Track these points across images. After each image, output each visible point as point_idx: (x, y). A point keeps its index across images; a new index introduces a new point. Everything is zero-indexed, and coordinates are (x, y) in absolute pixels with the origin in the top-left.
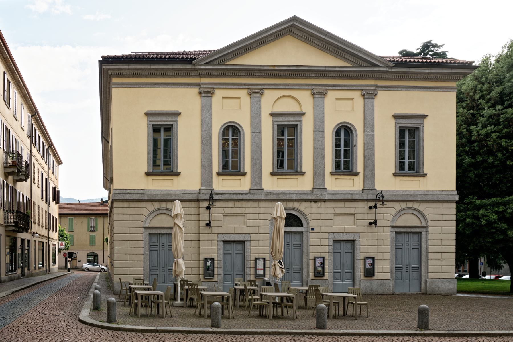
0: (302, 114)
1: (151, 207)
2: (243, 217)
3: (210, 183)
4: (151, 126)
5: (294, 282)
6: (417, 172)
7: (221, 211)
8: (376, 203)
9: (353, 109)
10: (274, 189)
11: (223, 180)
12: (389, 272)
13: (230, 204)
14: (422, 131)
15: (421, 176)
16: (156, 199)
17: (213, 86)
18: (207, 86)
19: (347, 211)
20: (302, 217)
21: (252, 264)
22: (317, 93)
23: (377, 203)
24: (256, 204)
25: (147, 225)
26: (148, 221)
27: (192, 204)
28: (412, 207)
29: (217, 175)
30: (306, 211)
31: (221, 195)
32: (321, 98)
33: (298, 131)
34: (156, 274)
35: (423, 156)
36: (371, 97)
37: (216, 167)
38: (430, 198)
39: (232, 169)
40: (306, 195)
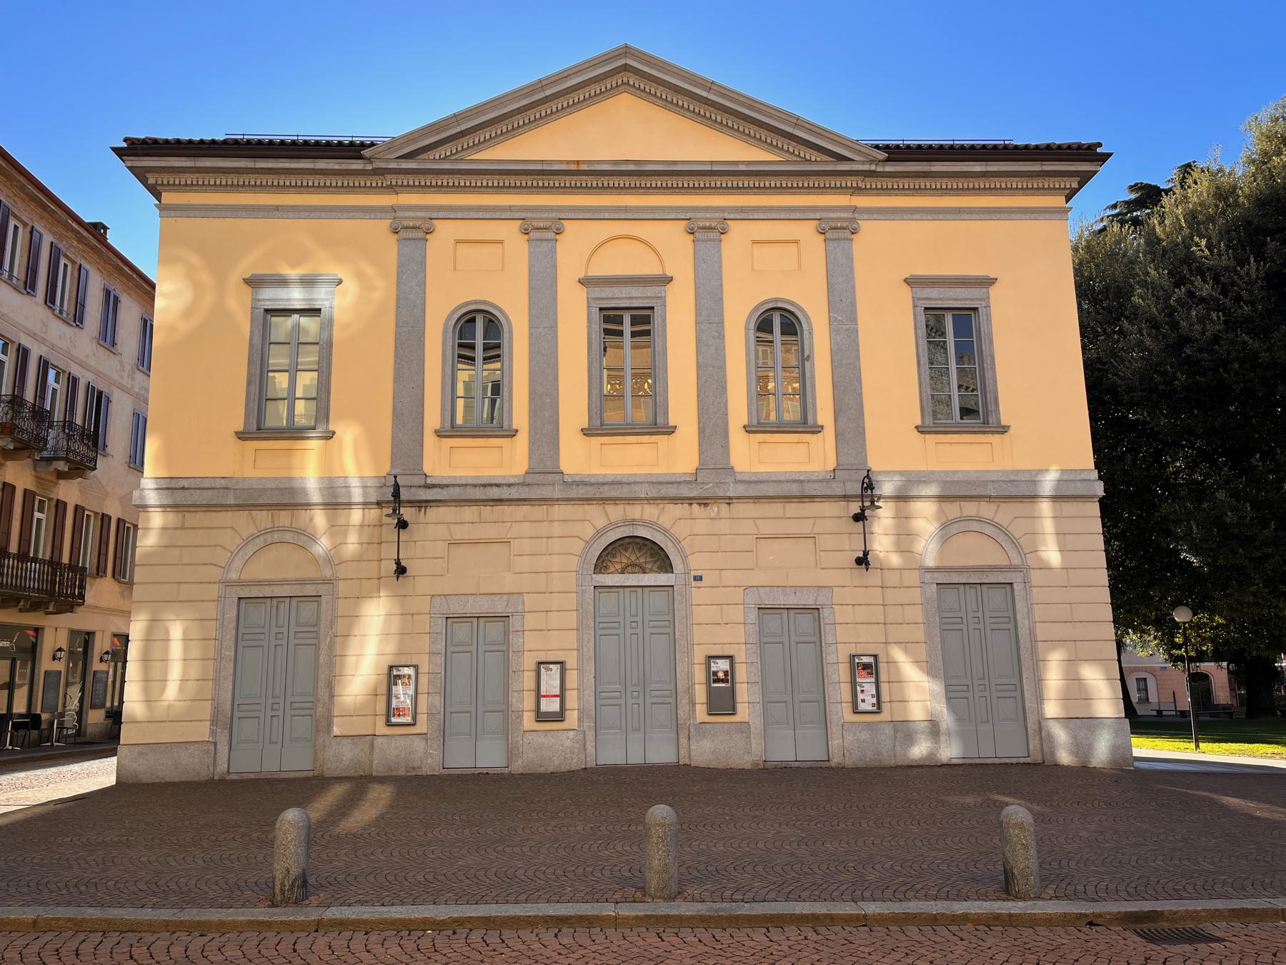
1: (244, 523)
4: (595, 311)
6: (986, 422)
7: (442, 531)
9: (800, 268)
13: (469, 513)
14: (985, 318)
15: (993, 433)
16: (261, 501)
17: (430, 215)
18: (412, 214)
19: (792, 527)
20: (670, 544)
24: (539, 512)
25: (234, 576)
26: (238, 563)
30: (680, 530)
31: (439, 490)
33: (656, 322)
35: (996, 382)
36: (841, 234)
37: (433, 418)
40: (675, 485)
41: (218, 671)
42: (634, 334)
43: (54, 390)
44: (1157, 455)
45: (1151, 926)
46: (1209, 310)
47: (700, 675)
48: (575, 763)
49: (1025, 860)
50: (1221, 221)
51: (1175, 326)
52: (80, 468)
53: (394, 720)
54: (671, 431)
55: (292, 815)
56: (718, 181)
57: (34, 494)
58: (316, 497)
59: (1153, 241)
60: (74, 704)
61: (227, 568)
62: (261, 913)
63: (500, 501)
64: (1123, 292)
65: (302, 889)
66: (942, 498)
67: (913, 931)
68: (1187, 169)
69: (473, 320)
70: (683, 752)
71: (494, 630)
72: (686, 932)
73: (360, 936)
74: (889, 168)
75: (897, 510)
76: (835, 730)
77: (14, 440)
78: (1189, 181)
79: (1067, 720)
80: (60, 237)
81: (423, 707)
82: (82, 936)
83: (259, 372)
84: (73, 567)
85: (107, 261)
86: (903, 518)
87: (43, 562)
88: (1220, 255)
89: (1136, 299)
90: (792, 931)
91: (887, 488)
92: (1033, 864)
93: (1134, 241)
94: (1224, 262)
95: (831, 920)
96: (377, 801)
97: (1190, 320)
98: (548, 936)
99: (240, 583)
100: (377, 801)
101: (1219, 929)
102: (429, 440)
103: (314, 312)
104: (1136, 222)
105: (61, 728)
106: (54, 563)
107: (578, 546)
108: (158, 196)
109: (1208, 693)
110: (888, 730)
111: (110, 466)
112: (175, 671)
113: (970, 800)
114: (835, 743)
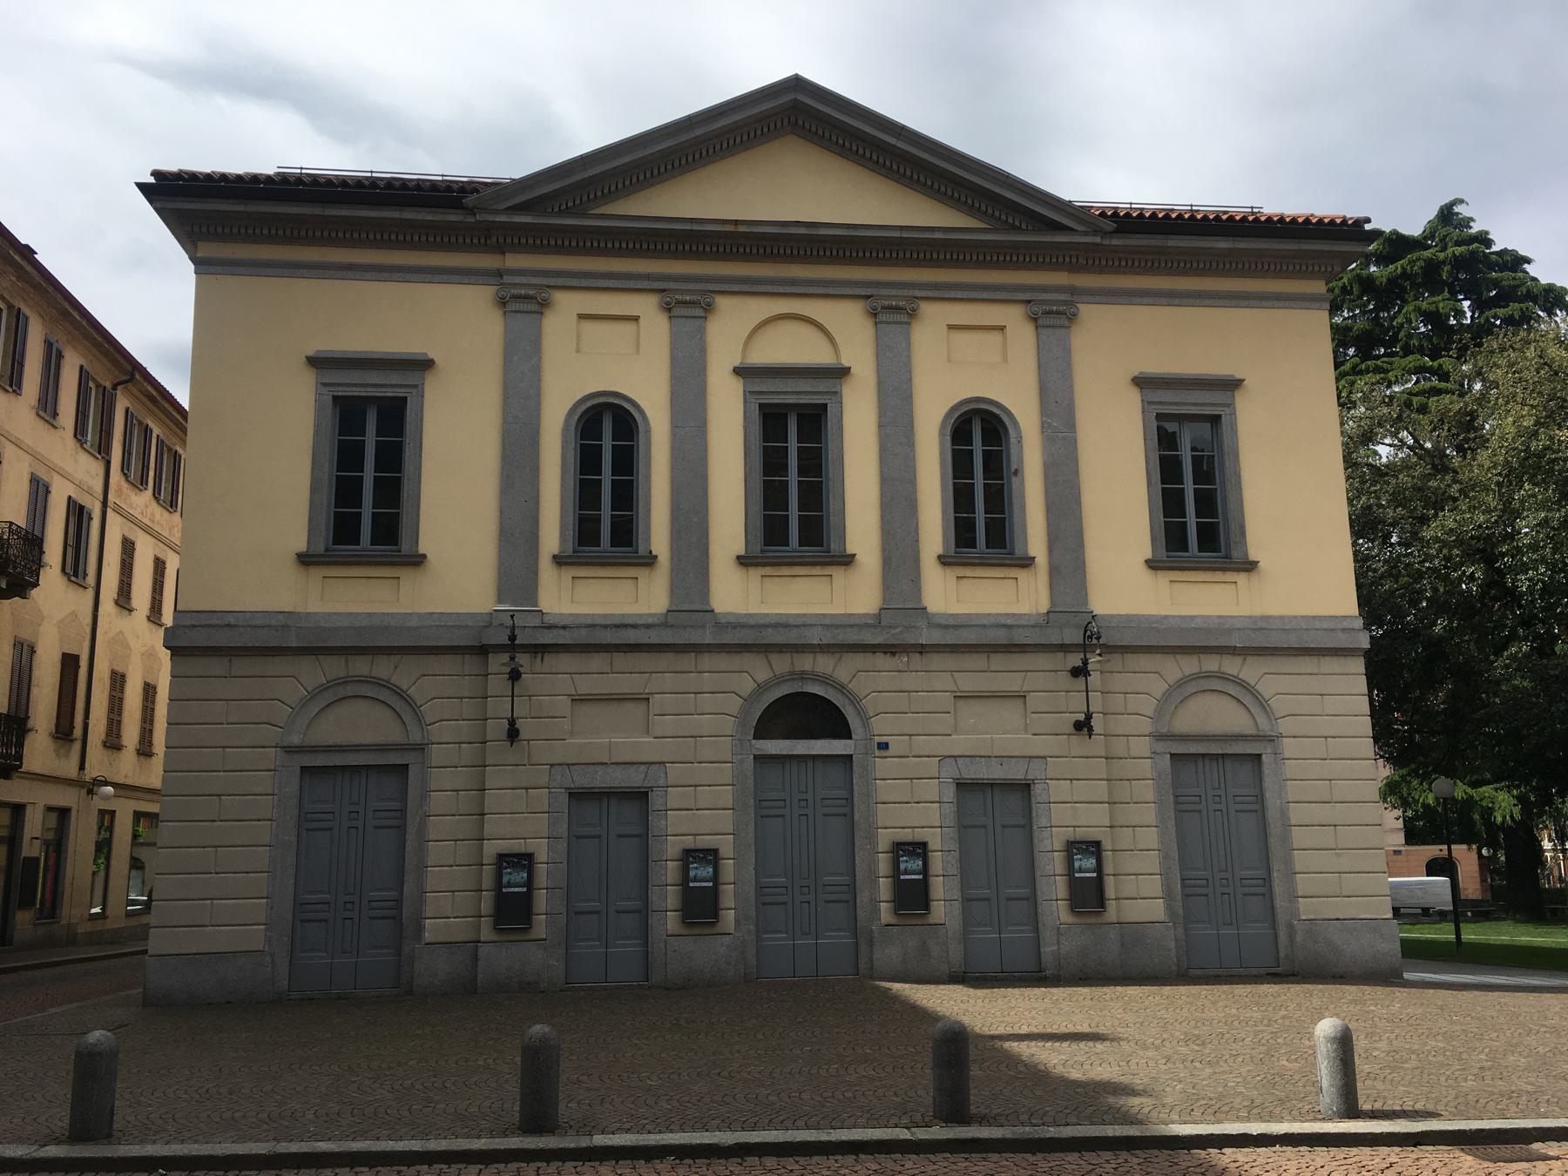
0: (842, 373)
1: (312, 673)
2: (643, 706)
5: (830, 937)
8: (1085, 656)
10: (751, 611)
11: (578, 581)
12: (1160, 894)
15: (1238, 570)
17: (546, 281)
18: (524, 280)
22: (883, 308)
23: (1088, 656)
24: (686, 661)
25: (295, 739)
27: (463, 662)
28: (1216, 669)
29: (554, 565)
32: (900, 323)
34: (320, 921)
37: (552, 533)
38: (1276, 640)
39: (800, 546)
102: (547, 571)
107: (734, 704)
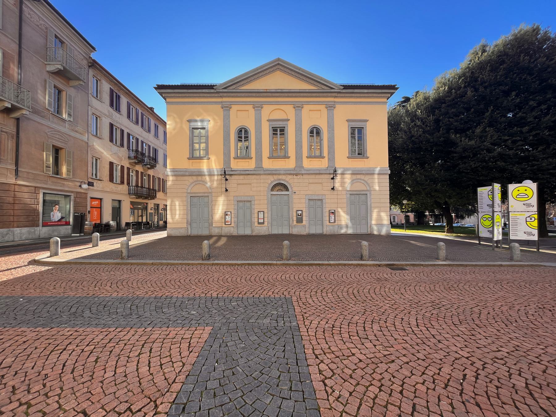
1: (191, 179)
3: (229, 163)
6: (364, 156)
13: (242, 177)
21: (256, 215)
24: (258, 177)
25: (189, 191)
26: (190, 188)
37: (233, 155)
41: (187, 212)
42: (280, 134)
43: (132, 142)
44: (403, 165)
45: (393, 267)
46: (419, 128)
47: (295, 214)
48: (267, 233)
49: (366, 253)
50: (425, 106)
51: (410, 132)
52: (153, 167)
53: (226, 223)
54: (289, 158)
55: (206, 242)
56: (301, 95)
57: (143, 173)
58: (206, 173)
59: (407, 111)
60: (156, 220)
61: (187, 189)
62: (200, 262)
63: (249, 174)
64: (398, 124)
65: (209, 257)
66: (352, 174)
67: (340, 267)
68: (417, 92)
69: (241, 131)
70: (291, 231)
71: (248, 204)
72: (291, 267)
73: (222, 267)
74: (344, 91)
75: (342, 177)
76: (325, 227)
77: (137, 160)
78: (418, 95)
79: (377, 225)
80: (143, 111)
81: (233, 221)
82: (163, 266)
83: (192, 144)
84: (153, 189)
85: (155, 117)
86: (343, 179)
87: (146, 188)
88: (423, 114)
89: (402, 126)
90: (314, 267)
91: (339, 172)
92: (367, 254)
93: (403, 111)
94: (424, 116)
95: (323, 265)
96: (223, 241)
97: (414, 131)
98: (262, 267)
99: (190, 193)
100: (223, 241)
101: (408, 268)
102: (232, 159)
103: (204, 128)
104: (403, 106)
105: (154, 224)
106: (149, 189)
107: (267, 185)
108: (165, 100)
109: (409, 219)
110: (337, 226)
111: (159, 166)
112: (178, 212)
113: (354, 241)
114: (325, 229)
